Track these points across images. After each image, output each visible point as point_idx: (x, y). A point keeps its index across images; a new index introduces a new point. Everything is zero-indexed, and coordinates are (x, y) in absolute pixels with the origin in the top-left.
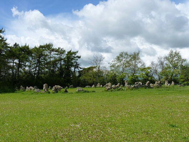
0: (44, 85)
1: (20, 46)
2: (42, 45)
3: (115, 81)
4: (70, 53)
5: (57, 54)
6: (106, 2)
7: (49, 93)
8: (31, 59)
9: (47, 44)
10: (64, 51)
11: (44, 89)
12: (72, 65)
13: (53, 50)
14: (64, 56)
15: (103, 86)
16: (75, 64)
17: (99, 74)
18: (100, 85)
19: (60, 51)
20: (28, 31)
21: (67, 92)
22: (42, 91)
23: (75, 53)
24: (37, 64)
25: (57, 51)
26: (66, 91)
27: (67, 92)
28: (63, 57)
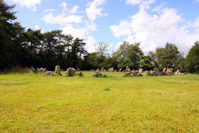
0: (56, 67)
1: (35, 31)
2: (54, 30)
3: (114, 64)
4: (77, 40)
5: (66, 40)
6: (151, 51)
7: (61, 75)
8: (42, 42)
9: (84, 44)
10: (72, 38)
11: (56, 71)
12: (78, 51)
13: (63, 36)
14: (72, 42)
15: (106, 70)
16: (81, 49)
17: (102, 59)
18: (104, 69)
19: (69, 38)
20: (176, 89)
21: (82, 75)
22: (54, 73)
23: (81, 40)
24: (47, 48)
25: (67, 37)
26: (81, 75)
27: (82, 75)
28: (71, 44)
